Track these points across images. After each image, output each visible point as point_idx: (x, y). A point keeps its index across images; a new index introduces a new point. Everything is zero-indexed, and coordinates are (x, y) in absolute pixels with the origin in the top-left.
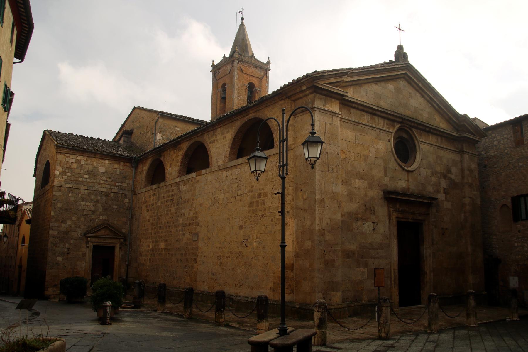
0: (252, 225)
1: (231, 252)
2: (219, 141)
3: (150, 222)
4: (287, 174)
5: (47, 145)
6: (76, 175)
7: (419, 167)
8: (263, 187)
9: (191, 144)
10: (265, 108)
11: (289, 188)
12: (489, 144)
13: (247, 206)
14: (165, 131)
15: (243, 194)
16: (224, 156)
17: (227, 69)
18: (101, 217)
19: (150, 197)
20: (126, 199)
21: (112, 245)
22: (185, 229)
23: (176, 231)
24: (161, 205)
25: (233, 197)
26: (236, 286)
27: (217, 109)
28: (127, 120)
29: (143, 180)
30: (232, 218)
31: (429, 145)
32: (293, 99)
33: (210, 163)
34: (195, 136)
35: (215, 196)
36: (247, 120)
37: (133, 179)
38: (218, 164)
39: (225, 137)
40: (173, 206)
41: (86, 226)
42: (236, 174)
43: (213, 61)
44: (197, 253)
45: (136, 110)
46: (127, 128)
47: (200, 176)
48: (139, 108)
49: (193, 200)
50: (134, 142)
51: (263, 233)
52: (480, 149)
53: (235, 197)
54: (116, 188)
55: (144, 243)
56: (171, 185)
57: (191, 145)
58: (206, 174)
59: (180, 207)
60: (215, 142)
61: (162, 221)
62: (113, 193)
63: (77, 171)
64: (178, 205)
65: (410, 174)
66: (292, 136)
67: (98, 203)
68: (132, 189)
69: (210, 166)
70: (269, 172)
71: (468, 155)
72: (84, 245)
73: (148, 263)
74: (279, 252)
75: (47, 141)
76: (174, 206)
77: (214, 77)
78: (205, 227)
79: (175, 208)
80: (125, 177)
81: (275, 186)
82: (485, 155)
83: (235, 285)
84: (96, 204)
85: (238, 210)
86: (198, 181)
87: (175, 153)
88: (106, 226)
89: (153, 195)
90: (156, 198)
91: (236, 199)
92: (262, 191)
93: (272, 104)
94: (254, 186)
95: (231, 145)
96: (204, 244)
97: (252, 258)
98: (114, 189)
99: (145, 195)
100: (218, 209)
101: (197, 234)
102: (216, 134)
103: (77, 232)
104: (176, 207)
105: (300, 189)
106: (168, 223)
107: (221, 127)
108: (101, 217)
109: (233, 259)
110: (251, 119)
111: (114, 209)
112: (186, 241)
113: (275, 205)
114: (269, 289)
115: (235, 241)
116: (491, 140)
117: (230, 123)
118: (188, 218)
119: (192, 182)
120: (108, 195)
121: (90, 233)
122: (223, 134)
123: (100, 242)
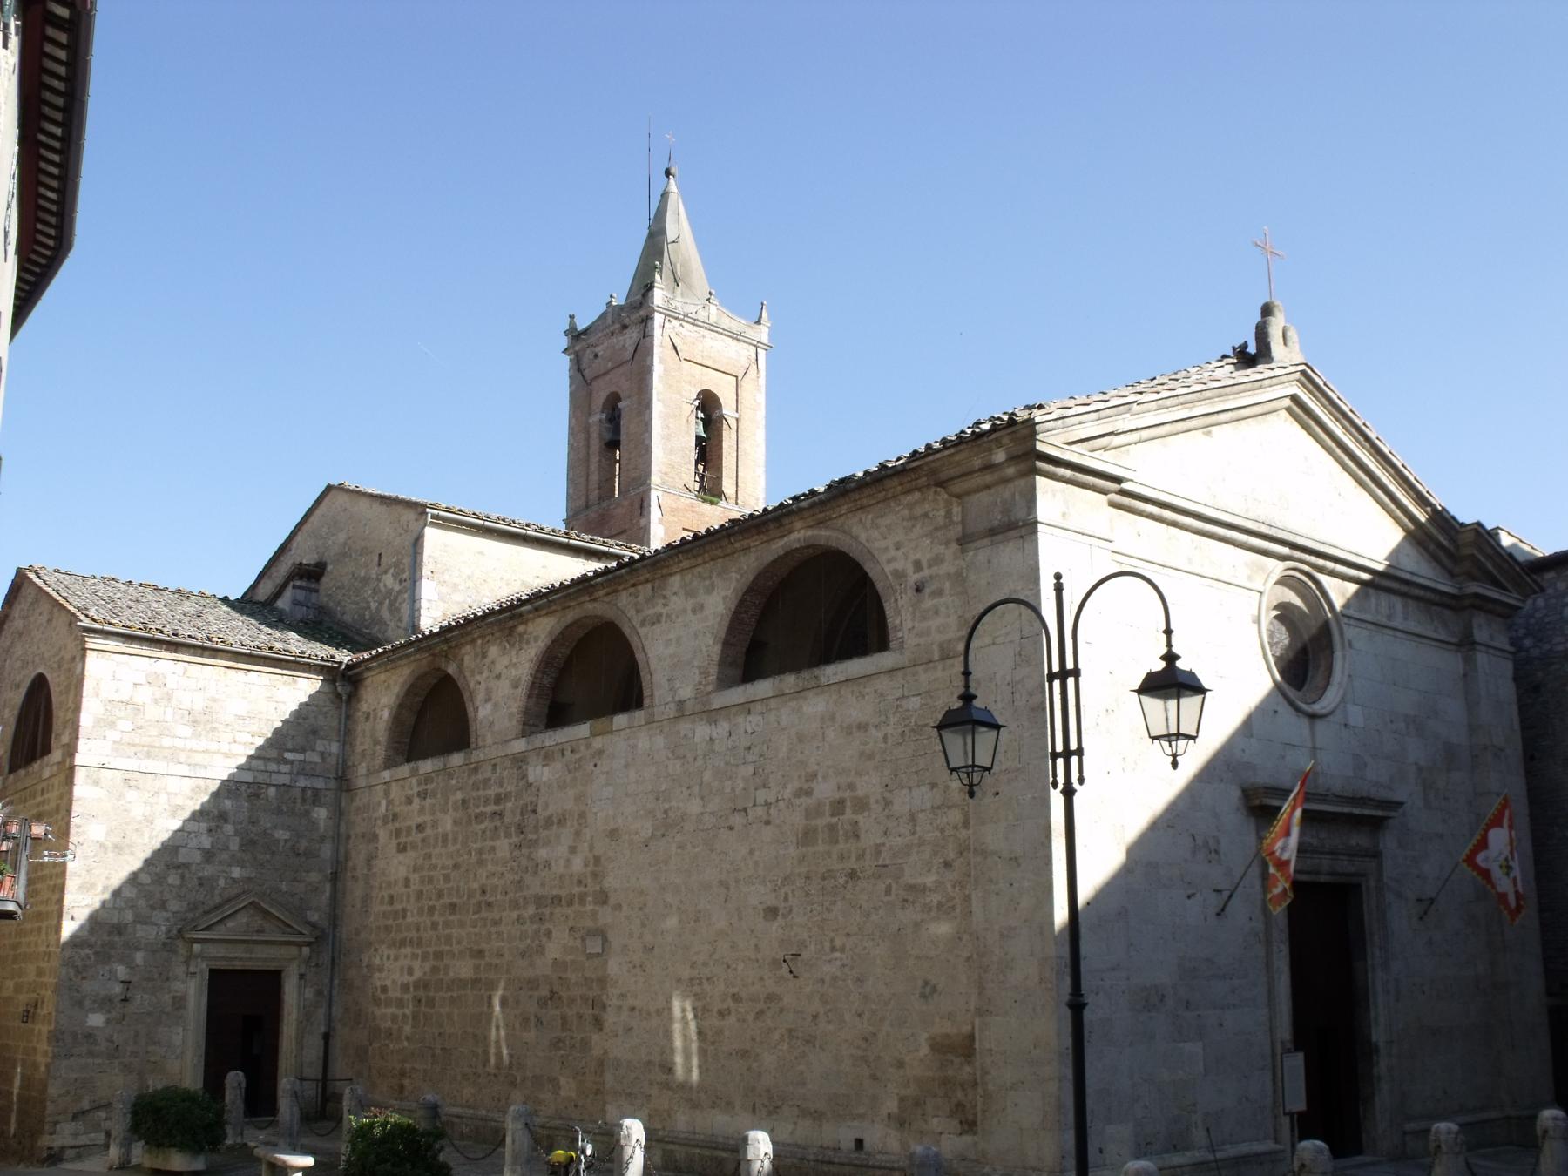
0: (813, 904)
1: (734, 995)
2: (677, 617)
3: (413, 887)
4: (1081, 780)
5: (32, 619)
6: (150, 726)
7: (1343, 700)
8: (849, 780)
9: (565, 624)
10: (849, 515)
11: (949, 783)
12: (1546, 615)
13: (795, 841)
14: (447, 570)
15: (778, 801)
16: (697, 671)
17: (624, 346)
18: (236, 872)
19: (409, 801)
20: (317, 808)
21: (272, 966)
22: (551, 914)
23: (518, 920)
24: (456, 829)
25: (739, 811)
26: (757, 1110)
27: (587, 480)
28: (299, 530)
29: (376, 742)
30: (737, 881)
31: (1370, 626)
32: (957, 487)
33: (646, 693)
34: (582, 599)
35: (667, 806)
36: (782, 553)
37: (342, 739)
38: (677, 699)
39: (702, 607)
40: (502, 834)
41: (185, 904)
42: (746, 732)
43: (572, 317)
44: (604, 997)
45: (333, 492)
46: (305, 554)
47: (609, 736)
48: (341, 488)
49: (582, 815)
50: (331, 604)
51: (855, 934)
52: (1516, 631)
53: (745, 810)
54: (285, 768)
55: (388, 958)
56: (493, 762)
57: (567, 627)
58: (630, 728)
59: (530, 840)
60: (664, 619)
61: (458, 887)
62: (274, 785)
63: (153, 712)
64: (522, 832)
65: (1320, 726)
66: (956, 612)
67: (226, 821)
68: (340, 774)
69: (646, 702)
70: (873, 731)
71: (1487, 653)
72: (180, 970)
73: (408, 1029)
74: (917, 996)
75: (32, 604)
76: (508, 835)
77: (578, 367)
78: (632, 909)
79: (511, 841)
80: (314, 732)
81: (896, 776)
82: (1535, 652)
83: (754, 1105)
84: (217, 826)
85: (757, 853)
86: (600, 752)
87: (504, 652)
88: (252, 903)
89: (423, 795)
90: (434, 805)
91: (750, 817)
92: (848, 794)
93: (878, 502)
94: (816, 775)
95: (723, 636)
96: (630, 965)
97: (815, 1017)
98: (279, 772)
99: (387, 793)
100: (679, 851)
101: (601, 934)
102: (664, 593)
103: (156, 925)
104: (515, 839)
105: (994, 791)
106: (484, 892)
107: (682, 570)
108: (236, 872)
109: (744, 1021)
110: (797, 549)
111: (278, 841)
112: (557, 956)
113: (898, 839)
114: (883, 1121)
115: (750, 959)
116: (1554, 601)
117: (719, 558)
118: (562, 877)
119: (577, 756)
120: (257, 796)
121: (200, 928)
122: (690, 594)
123: (235, 958)
